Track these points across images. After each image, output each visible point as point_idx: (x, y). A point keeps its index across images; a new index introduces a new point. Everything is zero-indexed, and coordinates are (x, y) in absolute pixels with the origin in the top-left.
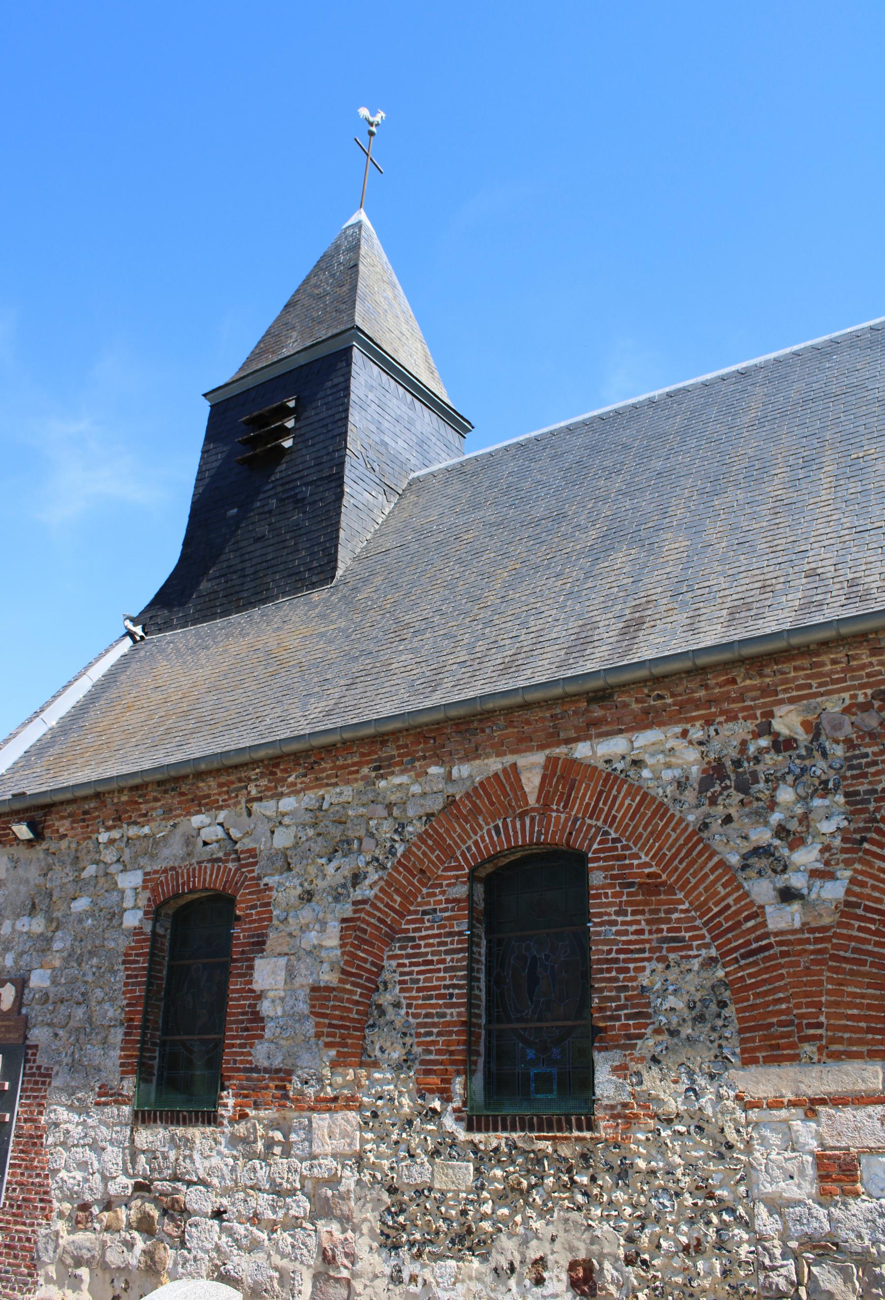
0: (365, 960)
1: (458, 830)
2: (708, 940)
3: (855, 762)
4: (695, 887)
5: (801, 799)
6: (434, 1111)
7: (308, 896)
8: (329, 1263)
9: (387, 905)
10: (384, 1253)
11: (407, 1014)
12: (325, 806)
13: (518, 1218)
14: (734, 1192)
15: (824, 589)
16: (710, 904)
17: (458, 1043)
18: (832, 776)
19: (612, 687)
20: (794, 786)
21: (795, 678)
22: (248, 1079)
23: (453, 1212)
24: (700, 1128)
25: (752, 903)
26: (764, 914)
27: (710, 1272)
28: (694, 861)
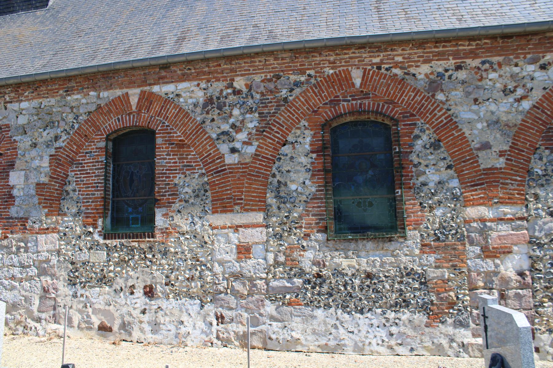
0: (61, 172)
1: (102, 119)
2: (202, 166)
3: (264, 101)
4: (198, 146)
5: (242, 114)
6: (90, 232)
7: (34, 145)
8: (46, 292)
9: (70, 150)
10: (70, 287)
11: (79, 194)
12: (42, 107)
13: (124, 271)
14: (206, 259)
15: (259, 33)
16: (204, 153)
17: (100, 205)
18: (255, 106)
19: (170, 64)
20: (240, 109)
21: (244, 67)
22: (7, 222)
23: (98, 270)
24: (195, 236)
25: (220, 153)
26: (224, 157)
27: (196, 286)
28: (198, 136)
